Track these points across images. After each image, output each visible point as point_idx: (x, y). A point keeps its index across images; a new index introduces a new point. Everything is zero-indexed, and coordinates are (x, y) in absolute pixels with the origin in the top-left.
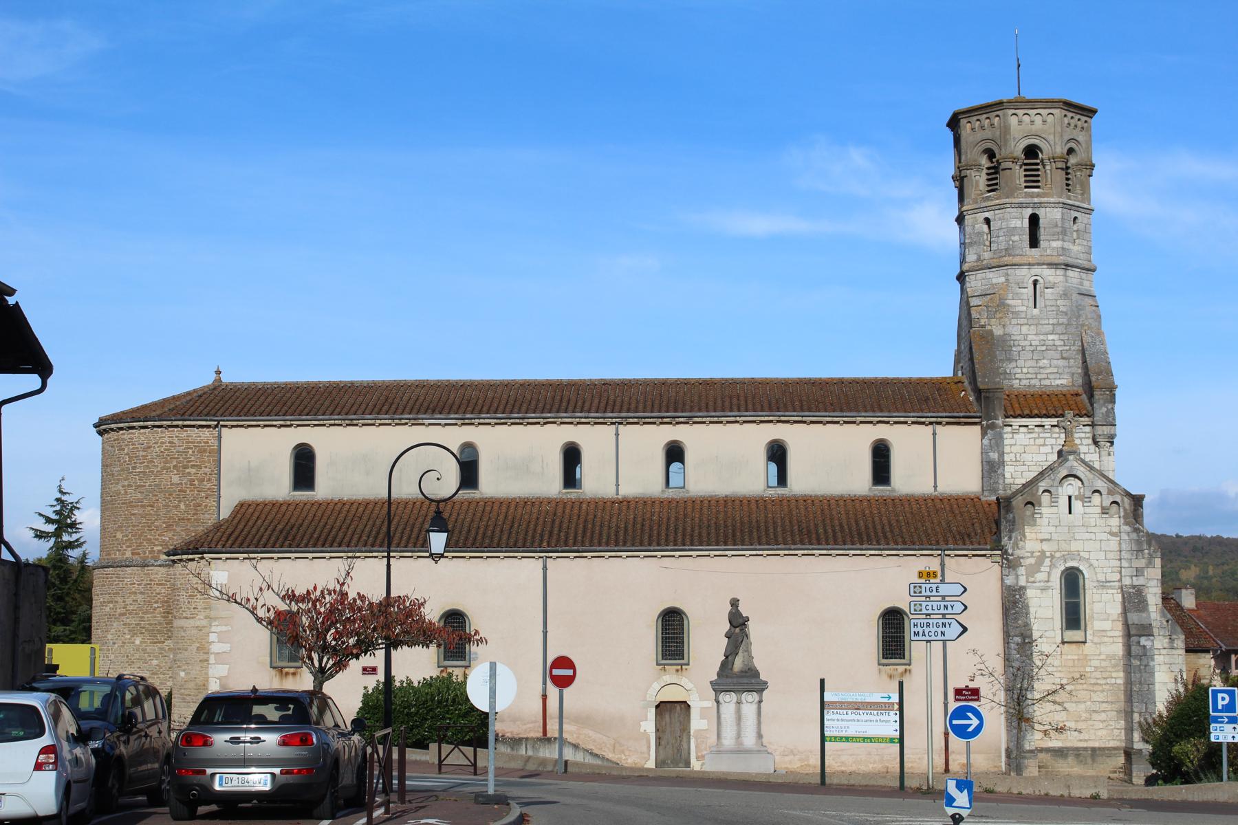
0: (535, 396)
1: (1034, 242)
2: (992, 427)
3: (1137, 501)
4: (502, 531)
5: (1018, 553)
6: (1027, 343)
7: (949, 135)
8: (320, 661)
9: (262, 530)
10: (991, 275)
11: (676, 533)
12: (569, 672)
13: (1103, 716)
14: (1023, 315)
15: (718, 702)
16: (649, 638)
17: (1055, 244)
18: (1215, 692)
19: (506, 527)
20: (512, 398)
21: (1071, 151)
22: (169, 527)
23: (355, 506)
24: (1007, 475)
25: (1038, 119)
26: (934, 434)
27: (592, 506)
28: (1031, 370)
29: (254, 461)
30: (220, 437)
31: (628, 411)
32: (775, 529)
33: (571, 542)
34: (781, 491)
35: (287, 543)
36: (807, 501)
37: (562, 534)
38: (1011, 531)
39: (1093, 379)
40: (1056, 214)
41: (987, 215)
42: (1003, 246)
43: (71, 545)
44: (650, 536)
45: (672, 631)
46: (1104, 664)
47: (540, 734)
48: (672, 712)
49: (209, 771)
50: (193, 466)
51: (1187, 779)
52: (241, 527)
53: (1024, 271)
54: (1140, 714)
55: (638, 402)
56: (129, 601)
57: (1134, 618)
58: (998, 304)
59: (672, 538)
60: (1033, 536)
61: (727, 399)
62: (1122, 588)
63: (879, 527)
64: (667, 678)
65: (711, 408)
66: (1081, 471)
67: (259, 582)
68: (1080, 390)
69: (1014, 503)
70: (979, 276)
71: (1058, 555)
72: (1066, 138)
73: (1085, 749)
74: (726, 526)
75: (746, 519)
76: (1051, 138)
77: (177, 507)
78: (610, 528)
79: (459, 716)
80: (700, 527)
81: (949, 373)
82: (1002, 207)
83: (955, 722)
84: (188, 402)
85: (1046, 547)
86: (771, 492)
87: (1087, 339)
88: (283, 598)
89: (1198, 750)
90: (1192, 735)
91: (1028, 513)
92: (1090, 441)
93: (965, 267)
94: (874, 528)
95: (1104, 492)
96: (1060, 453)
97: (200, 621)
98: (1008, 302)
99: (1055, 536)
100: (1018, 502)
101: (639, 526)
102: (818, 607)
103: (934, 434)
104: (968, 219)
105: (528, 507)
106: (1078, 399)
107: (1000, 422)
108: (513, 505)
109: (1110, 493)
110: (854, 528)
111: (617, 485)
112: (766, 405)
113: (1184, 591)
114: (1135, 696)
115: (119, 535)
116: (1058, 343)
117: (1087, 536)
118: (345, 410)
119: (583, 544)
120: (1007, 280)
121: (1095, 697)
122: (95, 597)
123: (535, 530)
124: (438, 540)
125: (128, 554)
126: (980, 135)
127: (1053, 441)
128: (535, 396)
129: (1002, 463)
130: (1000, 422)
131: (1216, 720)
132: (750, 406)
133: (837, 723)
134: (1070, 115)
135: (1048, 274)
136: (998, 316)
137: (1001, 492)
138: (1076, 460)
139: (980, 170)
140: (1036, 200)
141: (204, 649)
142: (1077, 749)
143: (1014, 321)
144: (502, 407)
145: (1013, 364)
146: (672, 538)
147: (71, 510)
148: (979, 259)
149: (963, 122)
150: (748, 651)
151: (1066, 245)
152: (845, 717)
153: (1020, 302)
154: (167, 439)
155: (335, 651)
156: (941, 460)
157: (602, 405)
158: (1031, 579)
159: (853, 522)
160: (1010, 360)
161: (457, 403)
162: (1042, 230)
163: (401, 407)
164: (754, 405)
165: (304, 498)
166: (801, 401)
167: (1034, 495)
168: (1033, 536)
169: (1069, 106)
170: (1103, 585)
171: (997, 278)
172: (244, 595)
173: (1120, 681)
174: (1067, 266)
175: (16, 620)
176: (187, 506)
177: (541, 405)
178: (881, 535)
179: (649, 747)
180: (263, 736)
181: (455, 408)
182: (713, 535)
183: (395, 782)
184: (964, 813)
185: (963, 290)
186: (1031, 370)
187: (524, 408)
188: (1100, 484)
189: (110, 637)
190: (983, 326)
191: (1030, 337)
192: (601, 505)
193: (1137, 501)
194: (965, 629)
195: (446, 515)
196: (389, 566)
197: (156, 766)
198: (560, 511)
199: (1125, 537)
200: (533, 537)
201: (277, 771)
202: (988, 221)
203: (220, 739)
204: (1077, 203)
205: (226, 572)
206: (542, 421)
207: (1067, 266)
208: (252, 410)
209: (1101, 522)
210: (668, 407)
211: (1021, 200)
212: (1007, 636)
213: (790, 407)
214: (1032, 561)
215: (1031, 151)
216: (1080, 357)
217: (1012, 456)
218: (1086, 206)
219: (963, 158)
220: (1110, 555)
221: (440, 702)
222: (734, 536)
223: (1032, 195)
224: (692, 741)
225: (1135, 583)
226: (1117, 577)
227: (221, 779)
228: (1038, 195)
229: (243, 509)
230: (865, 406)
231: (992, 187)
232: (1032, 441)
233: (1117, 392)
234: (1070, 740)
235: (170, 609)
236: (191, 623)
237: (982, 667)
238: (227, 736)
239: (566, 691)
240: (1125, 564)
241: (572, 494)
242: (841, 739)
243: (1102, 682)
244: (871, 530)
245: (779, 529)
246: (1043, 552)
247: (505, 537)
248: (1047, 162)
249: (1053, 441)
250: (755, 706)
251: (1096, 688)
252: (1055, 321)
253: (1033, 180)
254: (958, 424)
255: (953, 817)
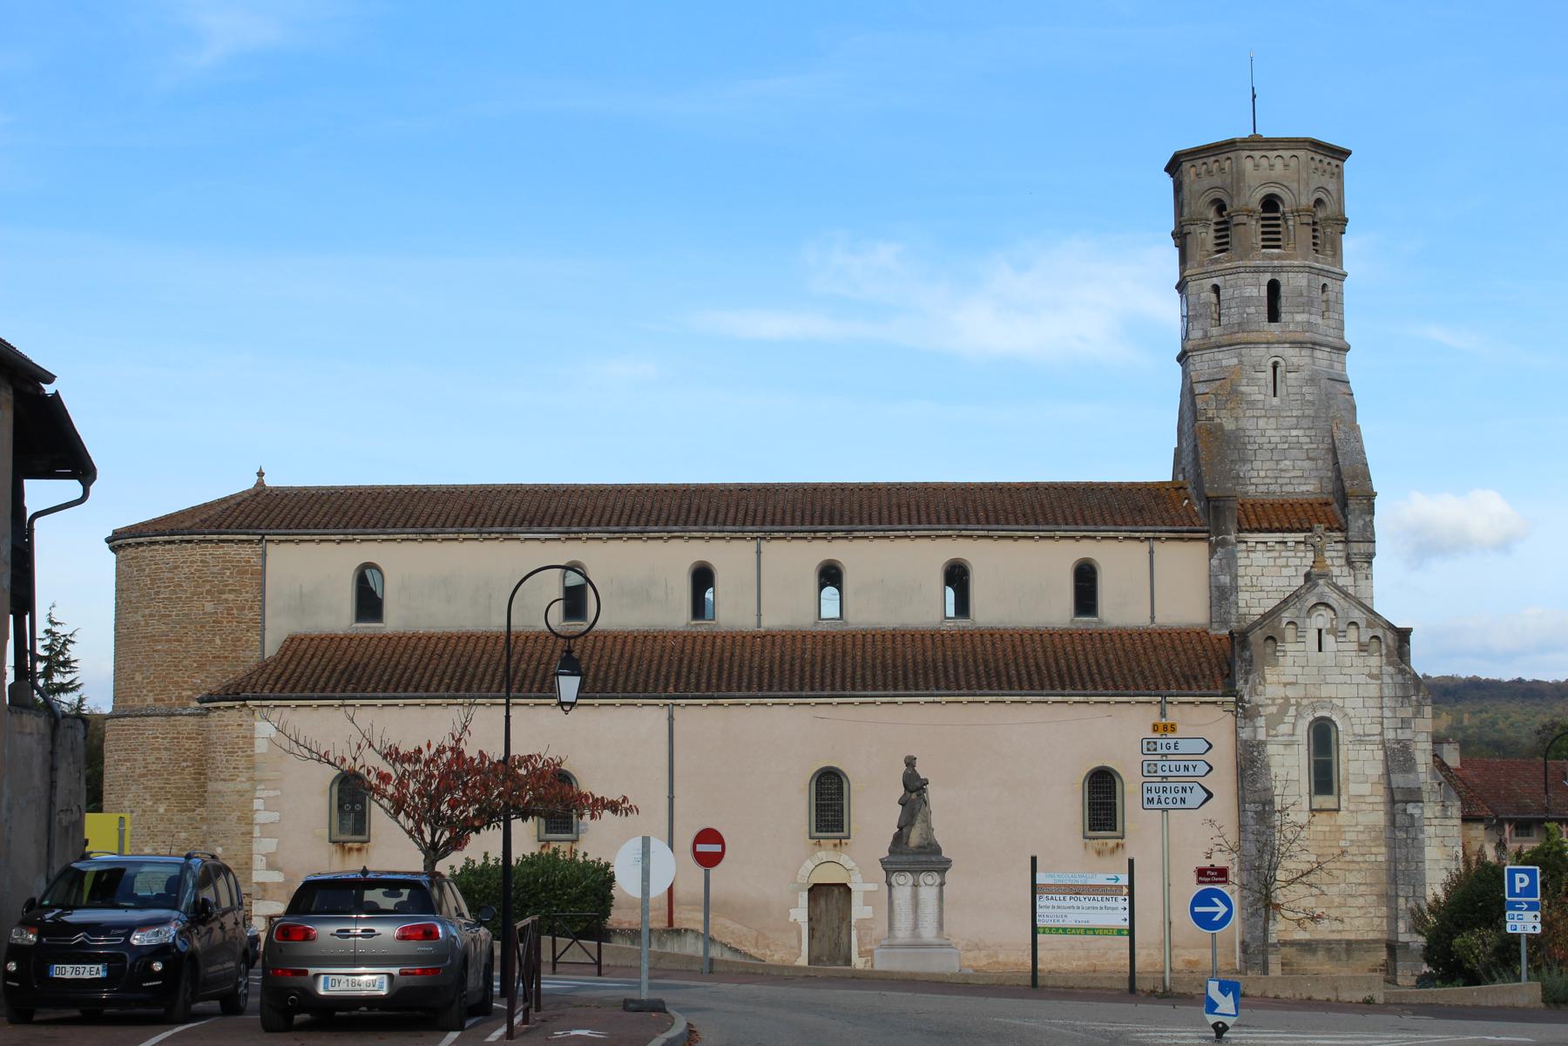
0: (657, 505)
1: (1274, 315)
2: (1223, 543)
3: (1403, 635)
4: (617, 673)
5: (1255, 699)
6: (1265, 440)
7: (1168, 182)
8: (433, 835)
9: (318, 671)
10: (1220, 356)
11: (432, 676)
12: (717, 848)
13: (1361, 901)
14: (1260, 405)
15: (890, 885)
16: (799, 806)
17: (1299, 318)
18: (1512, 873)
19: (624, 667)
20: (628, 507)
21: (1319, 202)
22: (201, 666)
23: (433, 642)
24: (1242, 604)
25: (1279, 164)
26: (1151, 552)
27: (729, 642)
28: (1270, 474)
29: (307, 586)
30: (264, 555)
31: (773, 523)
32: (956, 670)
33: (703, 686)
34: (962, 623)
35: (443, 687)
36: (993, 636)
37: (693, 676)
38: (1248, 673)
39: (1347, 484)
40: (1301, 280)
41: (1215, 281)
42: (1235, 319)
43: (63, 688)
44: (802, 679)
45: (829, 799)
46: (1361, 837)
47: (664, 925)
48: (829, 899)
49: (312, 971)
50: (231, 591)
51: (1472, 979)
52: (292, 667)
53: (1261, 351)
54: (1407, 899)
55: (784, 512)
56: (151, 759)
57: (1399, 780)
58: (1229, 393)
59: (828, 681)
60: (1275, 678)
61: (895, 509)
62: (1383, 743)
63: (1084, 668)
64: (823, 855)
65: (875, 519)
66: (1333, 598)
67: (357, 738)
68: (1331, 499)
69: (1251, 638)
70: (1206, 357)
71: (1305, 702)
72: (1313, 187)
73: (1338, 942)
74: (895, 666)
75: (919, 658)
76: (1294, 186)
77: (211, 641)
78: (751, 668)
79: (568, 902)
80: (863, 668)
81: (1167, 476)
82: (1235, 271)
83: (1197, 909)
84: (224, 511)
85: (1290, 692)
86: (950, 624)
87: (1338, 435)
88: (385, 757)
89: (1484, 944)
90: (1476, 924)
91: (1269, 650)
92: (1343, 562)
93: (1189, 346)
94: (1078, 668)
95: (1362, 624)
96: (1308, 576)
97: (242, 784)
98: (1243, 389)
99: (1301, 680)
100: (1256, 637)
101: (787, 666)
102: (1009, 766)
103: (1151, 552)
104: (1192, 287)
105: (649, 643)
106: (1327, 509)
107: (1232, 537)
108: (630, 640)
109: (1369, 625)
110: (1054, 669)
111: (759, 615)
112: (943, 516)
113: (1446, 746)
114: (1400, 876)
115: (138, 677)
116: (1302, 440)
117: (1342, 679)
118: (421, 521)
119: (718, 689)
120: (1241, 362)
121: (1351, 878)
122: (107, 754)
123: (658, 671)
124: (569, 686)
125: (150, 700)
126: (1207, 182)
127: (1298, 561)
128: (657, 505)
129: (1235, 589)
130: (1232, 537)
131: (1513, 906)
132: (924, 518)
133: (1052, 911)
134: (1318, 157)
135: (1291, 355)
136: (1229, 406)
137: (1234, 625)
138: (1328, 585)
139: (1206, 226)
140: (1276, 263)
141: (247, 819)
142: (1329, 942)
143: (1249, 413)
144: (615, 518)
145: (1248, 466)
146: (828, 681)
147: (64, 644)
148: (1205, 336)
149: (1186, 165)
150: (927, 821)
151: (1314, 319)
152: (1062, 903)
153: (1256, 389)
154: (198, 557)
155: (450, 824)
156: (1155, 586)
157: (740, 515)
158: (1272, 732)
159: (1051, 660)
160: (1244, 461)
161: (560, 512)
162: (1283, 300)
163: (490, 518)
164: (928, 515)
165: (370, 632)
166: (986, 511)
167: (1275, 628)
168: (1275, 678)
169: (1316, 146)
170: (1361, 739)
171: (1228, 359)
172: (339, 754)
173: (1381, 858)
174: (1315, 345)
175: (52, 785)
176: (223, 640)
177: (664, 516)
178: (1087, 678)
179: (800, 941)
180: (378, 928)
181: (557, 518)
182: (879, 677)
183: (497, 983)
184: (1229, 1021)
185: (1185, 374)
186: (1270, 474)
187: (643, 519)
188: (1357, 615)
189: (126, 803)
190: (1212, 419)
191: (1269, 433)
192: (737, 640)
193: (1403, 635)
194: (1210, 795)
195: (576, 655)
196: (508, 718)
197: (232, 964)
198: (688, 647)
199: (1387, 679)
200: (657, 679)
201: (395, 971)
202: (1216, 289)
203: (325, 931)
204: (1326, 267)
205: (266, 727)
206: (665, 535)
207: (1315, 345)
208: (305, 522)
209: (1358, 662)
210: (822, 518)
211: (1258, 263)
212: (1241, 801)
213: (973, 518)
214: (1274, 709)
215: (1270, 203)
216: (1330, 457)
217: (1247, 580)
218: (1337, 270)
219: (1186, 210)
220: (1370, 703)
221: (544, 885)
222: (905, 677)
223: (1271, 257)
224: (854, 933)
225: (1401, 737)
226: (1377, 729)
227: (326, 981)
228: (1279, 257)
229: (295, 646)
230: (1065, 518)
231: (1222, 247)
232: (1271, 562)
233: (1377, 501)
234: (1323, 931)
235: (202, 769)
236: (231, 785)
237: (1221, 841)
238: (334, 928)
239: (712, 871)
240: (1387, 713)
241: (703, 626)
242: (1057, 930)
243: (1360, 859)
244: (1075, 671)
245: (961, 670)
246: (1287, 699)
247: (621, 680)
248: (1289, 216)
249: (1298, 561)
250: (935, 890)
251: (1352, 866)
252: (1299, 413)
253: (1272, 238)
254: (1182, 539)
255: (1215, 1026)
